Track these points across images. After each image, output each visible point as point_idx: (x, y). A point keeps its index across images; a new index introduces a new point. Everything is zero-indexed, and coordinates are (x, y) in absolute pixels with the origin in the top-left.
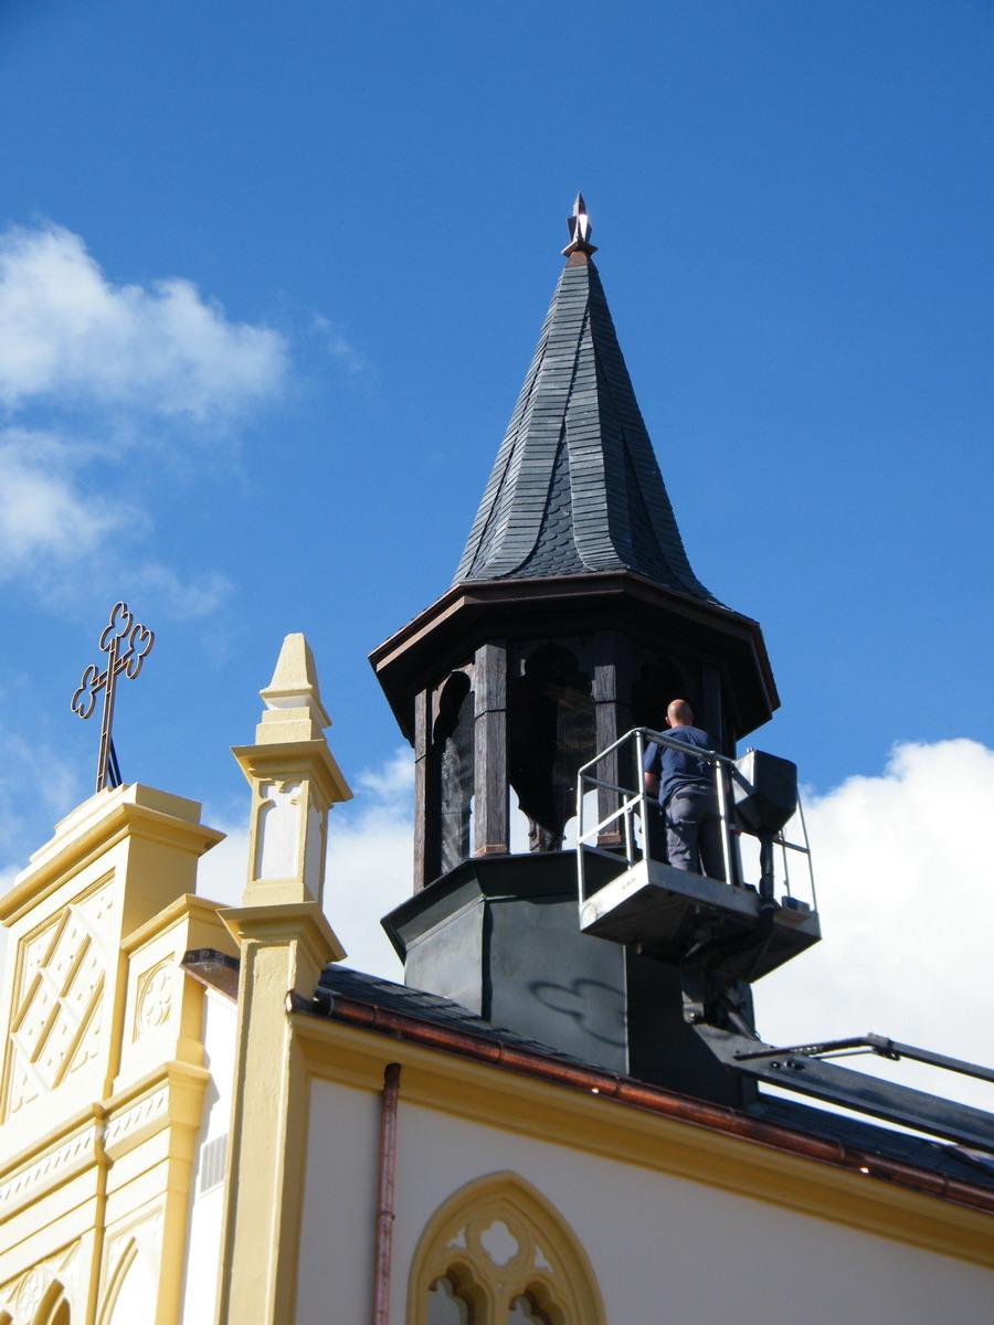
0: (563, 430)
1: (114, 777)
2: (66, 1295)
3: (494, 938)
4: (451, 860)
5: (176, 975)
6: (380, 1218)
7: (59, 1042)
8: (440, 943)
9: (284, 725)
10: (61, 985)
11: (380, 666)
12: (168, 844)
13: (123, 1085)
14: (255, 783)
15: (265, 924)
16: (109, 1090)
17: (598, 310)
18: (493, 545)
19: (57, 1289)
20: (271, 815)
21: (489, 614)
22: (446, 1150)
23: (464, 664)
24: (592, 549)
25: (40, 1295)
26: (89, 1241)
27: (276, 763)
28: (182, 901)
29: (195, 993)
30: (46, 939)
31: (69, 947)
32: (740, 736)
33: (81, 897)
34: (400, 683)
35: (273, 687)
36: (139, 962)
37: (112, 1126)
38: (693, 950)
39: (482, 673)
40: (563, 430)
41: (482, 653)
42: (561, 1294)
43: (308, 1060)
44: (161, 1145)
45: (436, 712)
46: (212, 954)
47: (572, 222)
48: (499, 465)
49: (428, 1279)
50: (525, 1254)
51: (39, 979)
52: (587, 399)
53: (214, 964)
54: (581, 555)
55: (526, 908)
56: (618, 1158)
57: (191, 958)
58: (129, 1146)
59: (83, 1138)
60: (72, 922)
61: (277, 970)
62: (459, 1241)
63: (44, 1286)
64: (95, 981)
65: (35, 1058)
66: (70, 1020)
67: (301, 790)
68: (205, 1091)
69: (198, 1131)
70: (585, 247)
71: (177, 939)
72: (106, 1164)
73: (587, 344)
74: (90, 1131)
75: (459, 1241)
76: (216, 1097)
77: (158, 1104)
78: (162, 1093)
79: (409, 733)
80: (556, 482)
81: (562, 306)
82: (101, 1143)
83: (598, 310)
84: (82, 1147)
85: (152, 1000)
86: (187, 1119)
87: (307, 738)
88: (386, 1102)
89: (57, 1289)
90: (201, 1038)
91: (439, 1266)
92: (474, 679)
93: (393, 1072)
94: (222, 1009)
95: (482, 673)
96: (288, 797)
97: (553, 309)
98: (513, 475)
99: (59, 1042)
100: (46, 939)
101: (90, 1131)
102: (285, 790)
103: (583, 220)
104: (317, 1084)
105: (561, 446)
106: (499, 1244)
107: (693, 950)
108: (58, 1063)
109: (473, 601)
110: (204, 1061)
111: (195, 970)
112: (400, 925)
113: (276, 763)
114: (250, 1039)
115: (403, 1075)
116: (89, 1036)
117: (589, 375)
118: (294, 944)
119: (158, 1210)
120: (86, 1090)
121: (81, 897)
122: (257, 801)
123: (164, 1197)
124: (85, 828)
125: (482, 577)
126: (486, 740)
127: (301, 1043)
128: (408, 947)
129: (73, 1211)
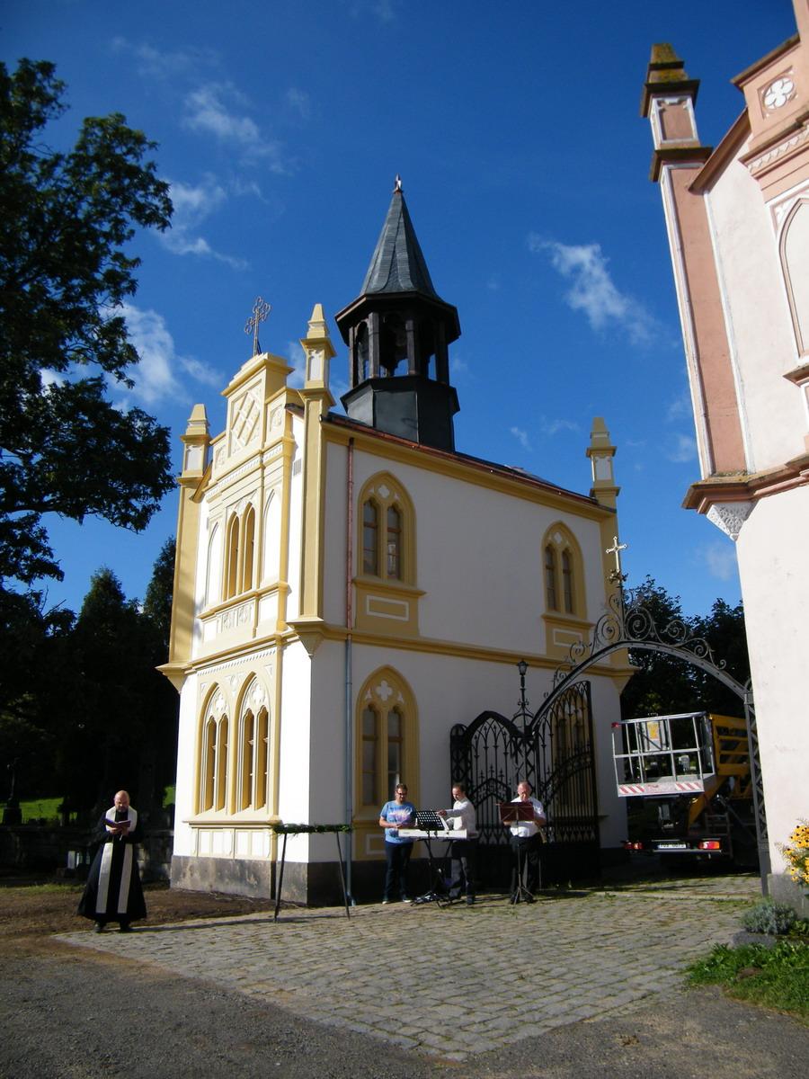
0: (395, 247)
1: (259, 352)
2: (237, 515)
3: (377, 402)
4: (361, 381)
5: (282, 411)
6: (349, 483)
7: (246, 433)
8: (358, 405)
9: (316, 332)
10: (246, 415)
12: (278, 373)
13: (267, 444)
14: (186, 445)
15: (313, 394)
16: (263, 446)
17: (405, 211)
18: (374, 280)
19: (250, 504)
20: (313, 361)
21: (375, 302)
22: (368, 465)
23: (364, 318)
24: (405, 284)
25: (245, 506)
26: (259, 490)
27: (314, 344)
28: (284, 388)
29: (289, 417)
30: (240, 402)
31: (247, 404)
32: (450, 342)
33: (251, 388)
34: (344, 326)
35: (312, 320)
36: (270, 407)
37: (265, 456)
38: (13, 784)
39: (370, 322)
40: (395, 247)
41: (371, 315)
42: (402, 506)
43: (327, 435)
44: (281, 462)
45: (356, 334)
46: (293, 405)
47: (396, 183)
48: (374, 257)
49: (364, 501)
51: (239, 414)
52: (402, 237)
53: (295, 408)
54: (402, 285)
55: (386, 394)
56: (418, 467)
57: (287, 406)
58: (270, 462)
59: (256, 460)
60: (249, 396)
61: (316, 408)
62: (372, 491)
64: (257, 414)
65: (239, 437)
66: (249, 426)
67: (322, 353)
68: (293, 446)
69: (292, 457)
70: (400, 191)
71: (283, 400)
72: (263, 468)
73: (402, 220)
74: (258, 458)
75: (372, 491)
76: (297, 447)
77: (279, 449)
78: (280, 447)
79: (347, 342)
80: (393, 263)
81: (393, 208)
82: (262, 461)
83: (405, 211)
84: (256, 462)
85: (275, 418)
86: (287, 454)
87: (323, 336)
88: (349, 449)
89: (250, 504)
90: (291, 429)
91: (366, 498)
92: (368, 323)
93: (351, 440)
94: (298, 423)
95: (370, 322)
96: (318, 355)
97: (390, 210)
98: (379, 261)
99: (246, 433)
100: (240, 402)
101: (258, 458)
102: (317, 353)
103: (399, 183)
104: (329, 443)
105: (394, 251)
106: (384, 492)
107: (13, 784)
108: (246, 439)
109: (369, 299)
110: (293, 437)
111: (290, 410)
112: (346, 400)
113: (314, 344)
114: (306, 431)
115: (355, 442)
116: (255, 431)
117: (402, 230)
118: (321, 401)
120: (256, 446)
121: (251, 388)
122: (308, 356)
123: (282, 478)
124: (252, 367)
125: (370, 291)
126: (372, 344)
127: (324, 430)
128: (349, 406)
129: (254, 482)
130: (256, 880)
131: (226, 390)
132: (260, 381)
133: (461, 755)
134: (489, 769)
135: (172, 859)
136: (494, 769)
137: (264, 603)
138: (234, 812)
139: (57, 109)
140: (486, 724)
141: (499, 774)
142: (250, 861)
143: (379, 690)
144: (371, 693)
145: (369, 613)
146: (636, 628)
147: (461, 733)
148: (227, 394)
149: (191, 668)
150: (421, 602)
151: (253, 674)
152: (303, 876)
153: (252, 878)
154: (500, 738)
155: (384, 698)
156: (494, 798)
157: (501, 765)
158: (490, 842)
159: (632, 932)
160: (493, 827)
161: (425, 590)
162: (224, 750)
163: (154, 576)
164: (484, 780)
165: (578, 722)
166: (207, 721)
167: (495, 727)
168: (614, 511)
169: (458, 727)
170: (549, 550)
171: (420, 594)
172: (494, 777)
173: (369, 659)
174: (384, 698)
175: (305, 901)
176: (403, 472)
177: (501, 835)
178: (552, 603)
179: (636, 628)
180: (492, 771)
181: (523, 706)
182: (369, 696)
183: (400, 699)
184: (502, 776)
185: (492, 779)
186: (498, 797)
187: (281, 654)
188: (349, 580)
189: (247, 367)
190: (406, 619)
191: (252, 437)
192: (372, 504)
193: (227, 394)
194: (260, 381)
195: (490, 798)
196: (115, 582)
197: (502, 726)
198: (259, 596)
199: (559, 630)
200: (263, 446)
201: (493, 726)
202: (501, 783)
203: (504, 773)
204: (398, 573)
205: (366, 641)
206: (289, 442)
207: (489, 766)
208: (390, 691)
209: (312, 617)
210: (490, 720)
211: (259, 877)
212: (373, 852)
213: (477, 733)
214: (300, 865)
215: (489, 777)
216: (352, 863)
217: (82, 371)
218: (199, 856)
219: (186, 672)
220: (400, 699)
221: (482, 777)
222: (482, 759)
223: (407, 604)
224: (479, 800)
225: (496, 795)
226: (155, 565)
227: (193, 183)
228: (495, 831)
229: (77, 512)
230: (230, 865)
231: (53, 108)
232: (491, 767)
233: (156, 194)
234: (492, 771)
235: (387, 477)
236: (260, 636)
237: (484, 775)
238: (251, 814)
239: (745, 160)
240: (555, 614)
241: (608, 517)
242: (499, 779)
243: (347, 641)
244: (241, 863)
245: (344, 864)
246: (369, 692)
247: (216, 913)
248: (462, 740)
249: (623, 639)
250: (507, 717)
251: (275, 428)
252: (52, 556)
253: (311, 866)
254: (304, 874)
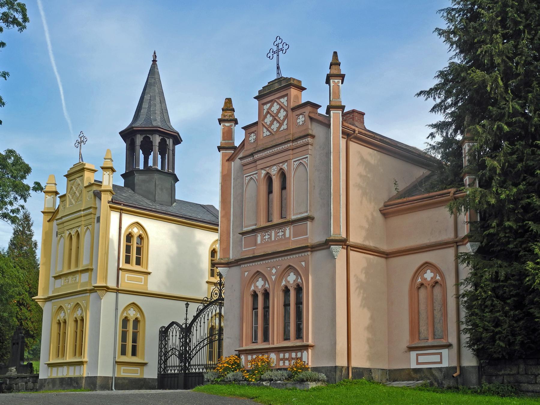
33: (78, 177)
42: (144, 235)
62: (130, 230)
133: (163, 338)
143: (426, 276)
147: (163, 330)
160: (173, 366)
165: (212, 326)
176: (146, 222)
181: (186, 320)
186: (176, 355)
190: (143, 283)
205: (378, 137)
208: (432, 275)
210: (175, 325)
222: (171, 341)
239: (240, 159)
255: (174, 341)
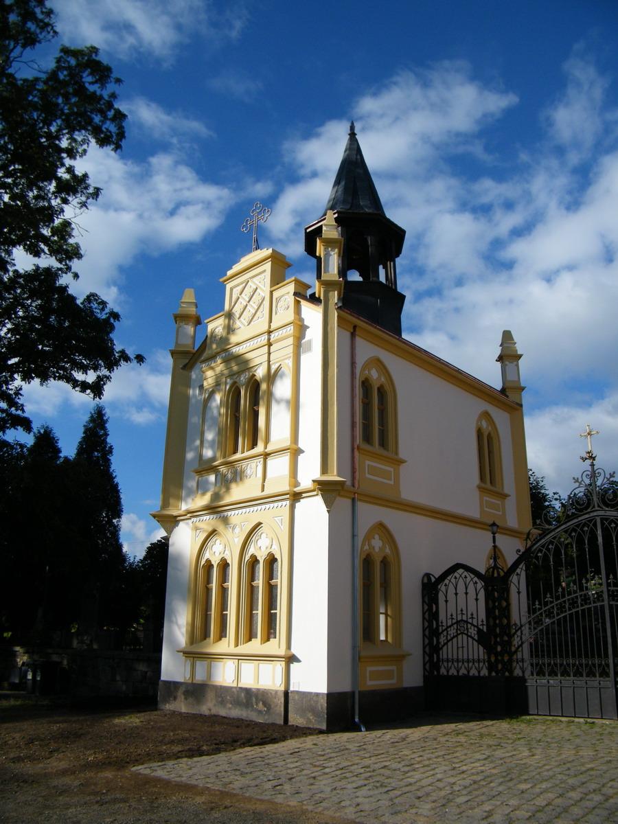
11: (308, 230)
16: (270, 327)
29: (297, 303)
31: (248, 291)
42: (387, 388)
50: (379, 378)
57: (295, 294)
58: (278, 341)
59: (263, 338)
63: (290, 370)
71: (291, 288)
72: (270, 345)
74: (266, 336)
77: (290, 330)
82: (269, 339)
86: (297, 335)
93: (355, 327)
106: (374, 374)
119: (290, 357)
130: (265, 706)
131: (225, 278)
132: (264, 271)
134: (459, 612)
135: (160, 683)
136: (464, 612)
137: (271, 462)
138: (237, 645)
139: (51, 33)
140: (456, 574)
141: (469, 616)
142: (258, 690)
144: (369, 545)
145: (367, 475)
146: (608, 499)
148: (225, 281)
149: (186, 515)
150: (403, 467)
151: (260, 524)
152: (322, 705)
153: (261, 704)
154: (471, 587)
155: (377, 549)
156: (465, 637)
157: (472, 608)
158: (471, 674)
159: (544, 786)
161: (406, 459)
162: (224, 592)
163: (83, 435)
164: (454, 621)
166: (202, 563)
167: (466, 577)
168: (521, 406)
169: (428, 575)
170: (480, 433)
171: (403, 462)
172: (465, 618)
173: (369, 514)
174: (377, 549)
175: (324, 727)
177: (482, 668)
178: (482, 478)
179: (608, 499)
180: (462, 614)
182: (366, 547)
183: (388, 550)
184: (472, 618)
185: (462, 620)
187: (292, 508)
188: (356, 446)
189: (246, 261)
191: (254, 320)
192: (366, 384)
193: (225, 281)
194: (264, 271)
195: (460, 637)
196: (54, 438)
197: (473, 576)
198: (266, 455)
199: (488, 499)
200: (270, 327)
201: (463, 576)
202: (472, 624)
203: (475, 616)
204: (383, 443)
206: (299, 325)
207: (459, 609)
209: (333, 477)
210: (461, 571)
211: (270, 705)
212: (372, 683)
213: (446, 581)
214: (317, 695)
215: (459, 618)
216: (359, 692)
217: (47, 261)
218: (194, 682)
219: (179, 518)
220: (388, 550)
221: (452, 619)
223: (392, 470)
224: (449, 638)
225: (467, 635)
226: (84, 426)
227: (8, 139)
228: (456, 664)
229: (44, 378)
230: (233, 692)
231: (49, 32)
232: (462, 610)
233: (113, 120)
234: (462, 614)
235: (379, 363)
236: (267, 492)
237: (454, 617)
238: (255, 646)
240: (483, 485)
241: (516, 409)
242: (470, 621)
243: (353, 500)
244: (248, 691)
245: (353, 693)
246: (367, 544)
247: (256, 741)
248: (430, 588)
249: (597, 508)
250: (480, 571)
251: (281, 311)
252: (23, 411)
253: (330, 696)
254: (323, 703)
255: (462, 604)
